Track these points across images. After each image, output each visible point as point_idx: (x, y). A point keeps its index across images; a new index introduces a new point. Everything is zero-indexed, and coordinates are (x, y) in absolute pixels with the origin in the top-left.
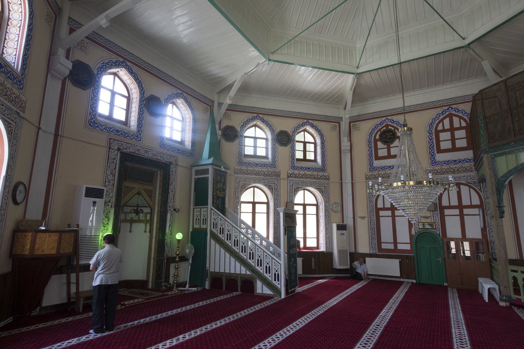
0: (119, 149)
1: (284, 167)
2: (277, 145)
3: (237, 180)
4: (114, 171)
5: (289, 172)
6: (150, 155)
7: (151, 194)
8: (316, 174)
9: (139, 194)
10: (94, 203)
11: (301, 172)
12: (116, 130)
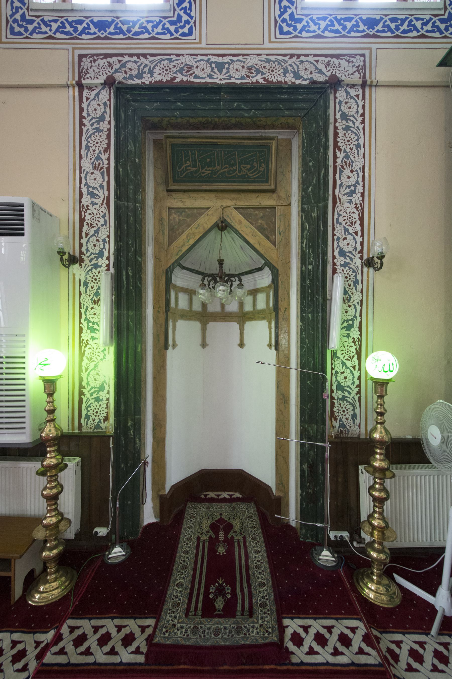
0: (109, 82)
4: (104, 157)
6: (236, 76)
7: (268, 222)
9: (223, 226)
12: (96, 25)
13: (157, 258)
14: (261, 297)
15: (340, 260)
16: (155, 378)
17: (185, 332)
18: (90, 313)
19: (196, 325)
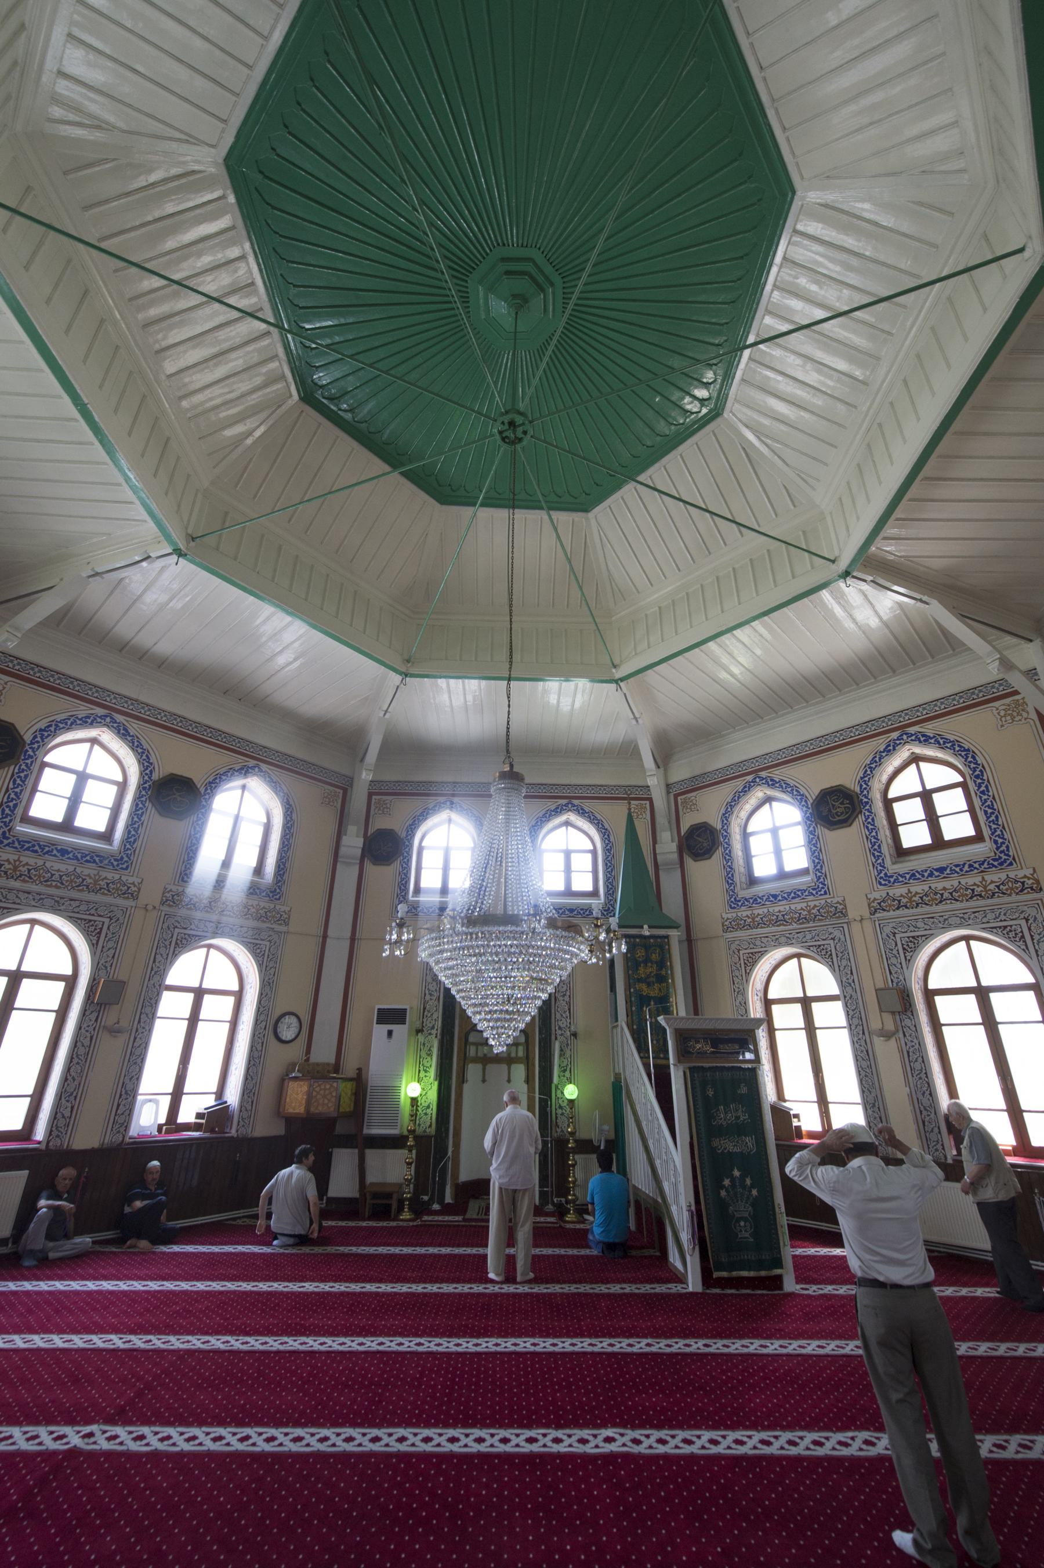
1: (854, 885)
2: (821, 830)
3: (733, 947)
5: (871, 896)
8: (978, 880)
10: (390, 1033)
11: (913, 889)
13: (460, 1026)
14: (521, 1048)
15: (559, 1032)
16: (456, 1102)
17: (473, 1070)
18: (425, 1061)
19: (479, 1066)
